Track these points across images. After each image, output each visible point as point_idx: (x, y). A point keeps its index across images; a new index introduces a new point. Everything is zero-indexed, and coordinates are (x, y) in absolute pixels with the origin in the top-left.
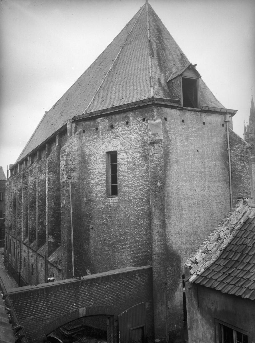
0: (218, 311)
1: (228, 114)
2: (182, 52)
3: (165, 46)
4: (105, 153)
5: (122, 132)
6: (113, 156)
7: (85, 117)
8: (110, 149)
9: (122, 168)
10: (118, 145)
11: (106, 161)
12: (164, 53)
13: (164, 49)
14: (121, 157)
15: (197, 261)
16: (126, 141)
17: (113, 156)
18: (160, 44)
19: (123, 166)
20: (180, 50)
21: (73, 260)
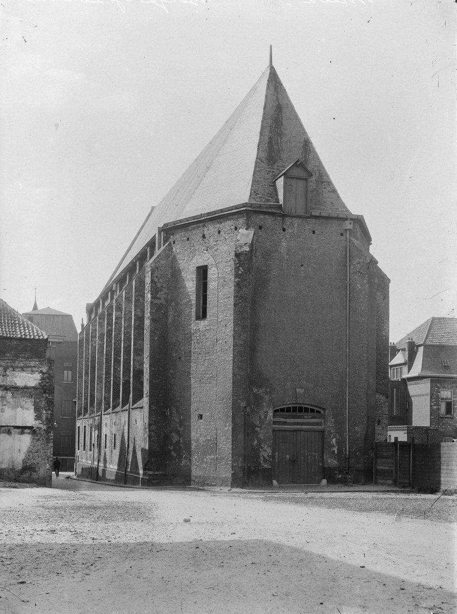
0: (79, 330)
1: (349, 219)
2: (307, 136)
3: (284, 131)
4: (195, 268)
5: (214, 243)
6: (203, 272)
7: (257, 498)
8: (201, 263)
9: (212, 285)
10: (209, 258)
11: (197, 278)
12: (279, 140)
13: (280, 135)
14: (212, 273)
15: (19, 409)
16: (217, 254)
17: (203, 272)
18: (277, 128)
19: (213, 283)
20: (305, 133)
21: (133, 323)
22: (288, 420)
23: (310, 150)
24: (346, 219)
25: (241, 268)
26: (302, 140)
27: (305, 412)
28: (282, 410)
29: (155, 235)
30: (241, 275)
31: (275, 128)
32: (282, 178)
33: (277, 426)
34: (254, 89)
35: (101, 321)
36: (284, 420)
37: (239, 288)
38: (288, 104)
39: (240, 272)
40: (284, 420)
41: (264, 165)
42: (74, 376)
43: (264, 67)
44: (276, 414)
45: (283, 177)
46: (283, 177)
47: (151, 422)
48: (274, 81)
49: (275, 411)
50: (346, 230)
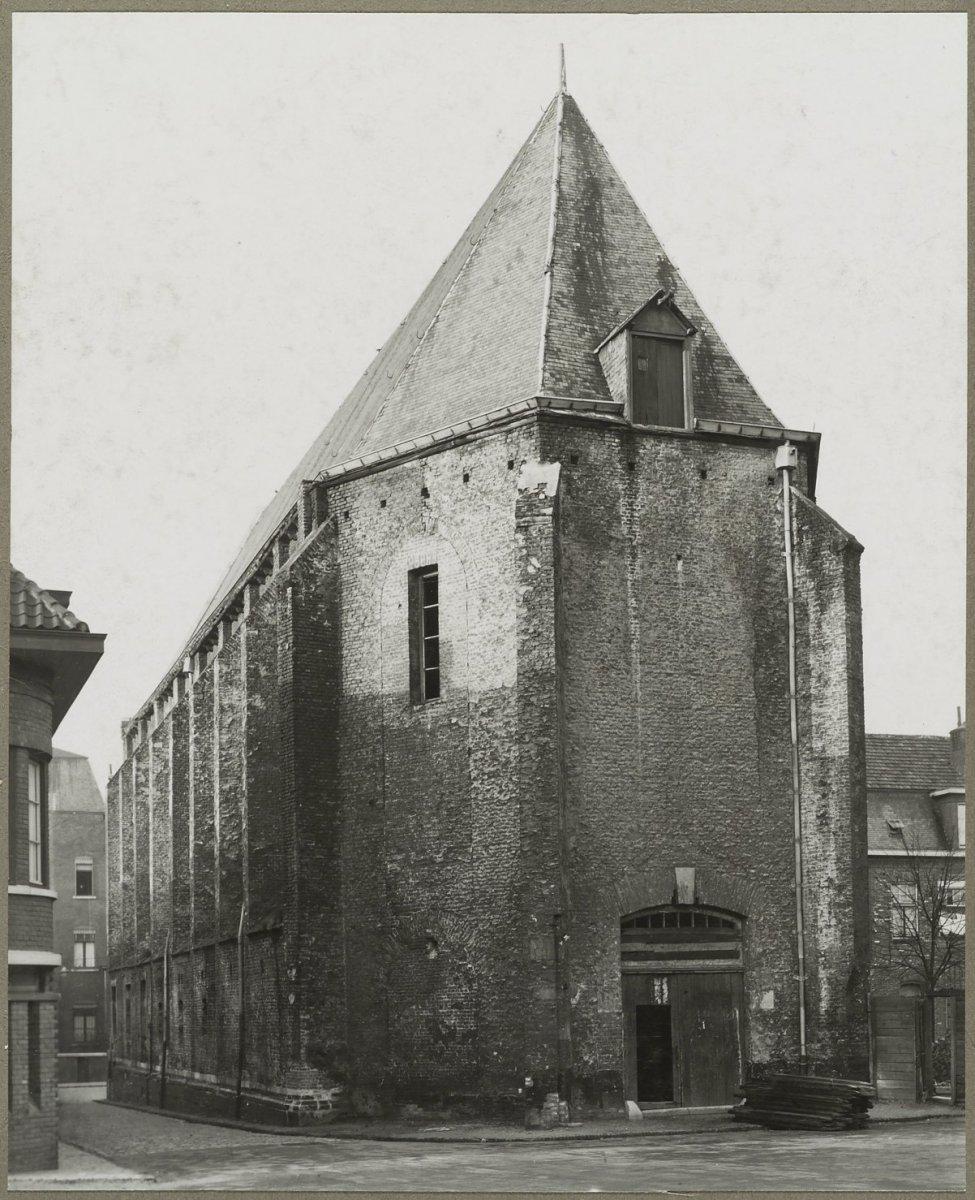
6: (424, 584)
13: (602, 246)
17: (424, 584)
18: (592, 231)
22: (658, 948)
23: (675, 284)
24: (781, 442)
25: (534, 561)
26: (654, 261)
27: (653, 926)
28: (641, 922)
29: (294, 510)
30: (535, 577)
31: (587, 229)
32: (622, 341)
33: (633, 964)
34: (497, 207)
35: (159, 745)
36: (648, 948)
37: (529, 610)
38: (611, 179)
39: (531, 570)
40: (648, 948)
41: (567, 313)
42: (99, 1024)
43: (555, 89)
44: (628, 932)
45: (624, 335)
46: (624, 335)
47: (26, 862)
48: (573, 121)
49: (625, 925)
50: (782, 468)
